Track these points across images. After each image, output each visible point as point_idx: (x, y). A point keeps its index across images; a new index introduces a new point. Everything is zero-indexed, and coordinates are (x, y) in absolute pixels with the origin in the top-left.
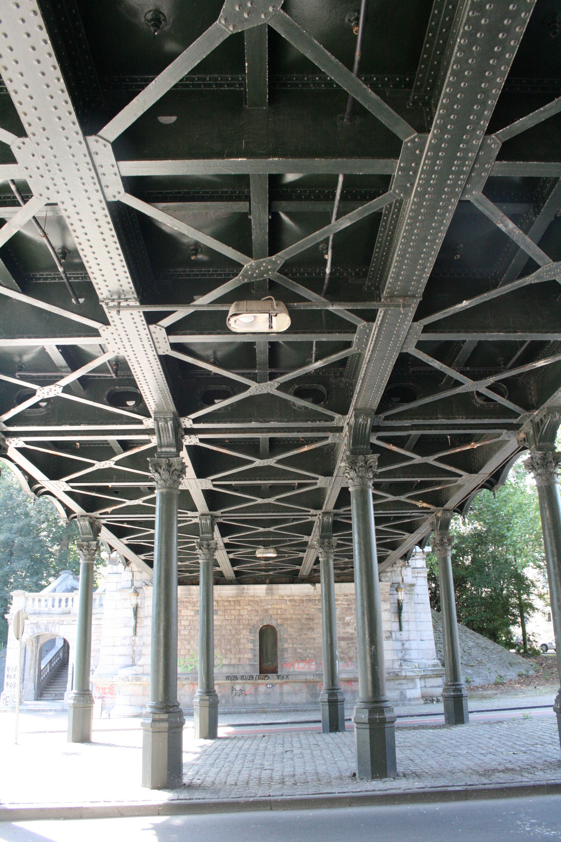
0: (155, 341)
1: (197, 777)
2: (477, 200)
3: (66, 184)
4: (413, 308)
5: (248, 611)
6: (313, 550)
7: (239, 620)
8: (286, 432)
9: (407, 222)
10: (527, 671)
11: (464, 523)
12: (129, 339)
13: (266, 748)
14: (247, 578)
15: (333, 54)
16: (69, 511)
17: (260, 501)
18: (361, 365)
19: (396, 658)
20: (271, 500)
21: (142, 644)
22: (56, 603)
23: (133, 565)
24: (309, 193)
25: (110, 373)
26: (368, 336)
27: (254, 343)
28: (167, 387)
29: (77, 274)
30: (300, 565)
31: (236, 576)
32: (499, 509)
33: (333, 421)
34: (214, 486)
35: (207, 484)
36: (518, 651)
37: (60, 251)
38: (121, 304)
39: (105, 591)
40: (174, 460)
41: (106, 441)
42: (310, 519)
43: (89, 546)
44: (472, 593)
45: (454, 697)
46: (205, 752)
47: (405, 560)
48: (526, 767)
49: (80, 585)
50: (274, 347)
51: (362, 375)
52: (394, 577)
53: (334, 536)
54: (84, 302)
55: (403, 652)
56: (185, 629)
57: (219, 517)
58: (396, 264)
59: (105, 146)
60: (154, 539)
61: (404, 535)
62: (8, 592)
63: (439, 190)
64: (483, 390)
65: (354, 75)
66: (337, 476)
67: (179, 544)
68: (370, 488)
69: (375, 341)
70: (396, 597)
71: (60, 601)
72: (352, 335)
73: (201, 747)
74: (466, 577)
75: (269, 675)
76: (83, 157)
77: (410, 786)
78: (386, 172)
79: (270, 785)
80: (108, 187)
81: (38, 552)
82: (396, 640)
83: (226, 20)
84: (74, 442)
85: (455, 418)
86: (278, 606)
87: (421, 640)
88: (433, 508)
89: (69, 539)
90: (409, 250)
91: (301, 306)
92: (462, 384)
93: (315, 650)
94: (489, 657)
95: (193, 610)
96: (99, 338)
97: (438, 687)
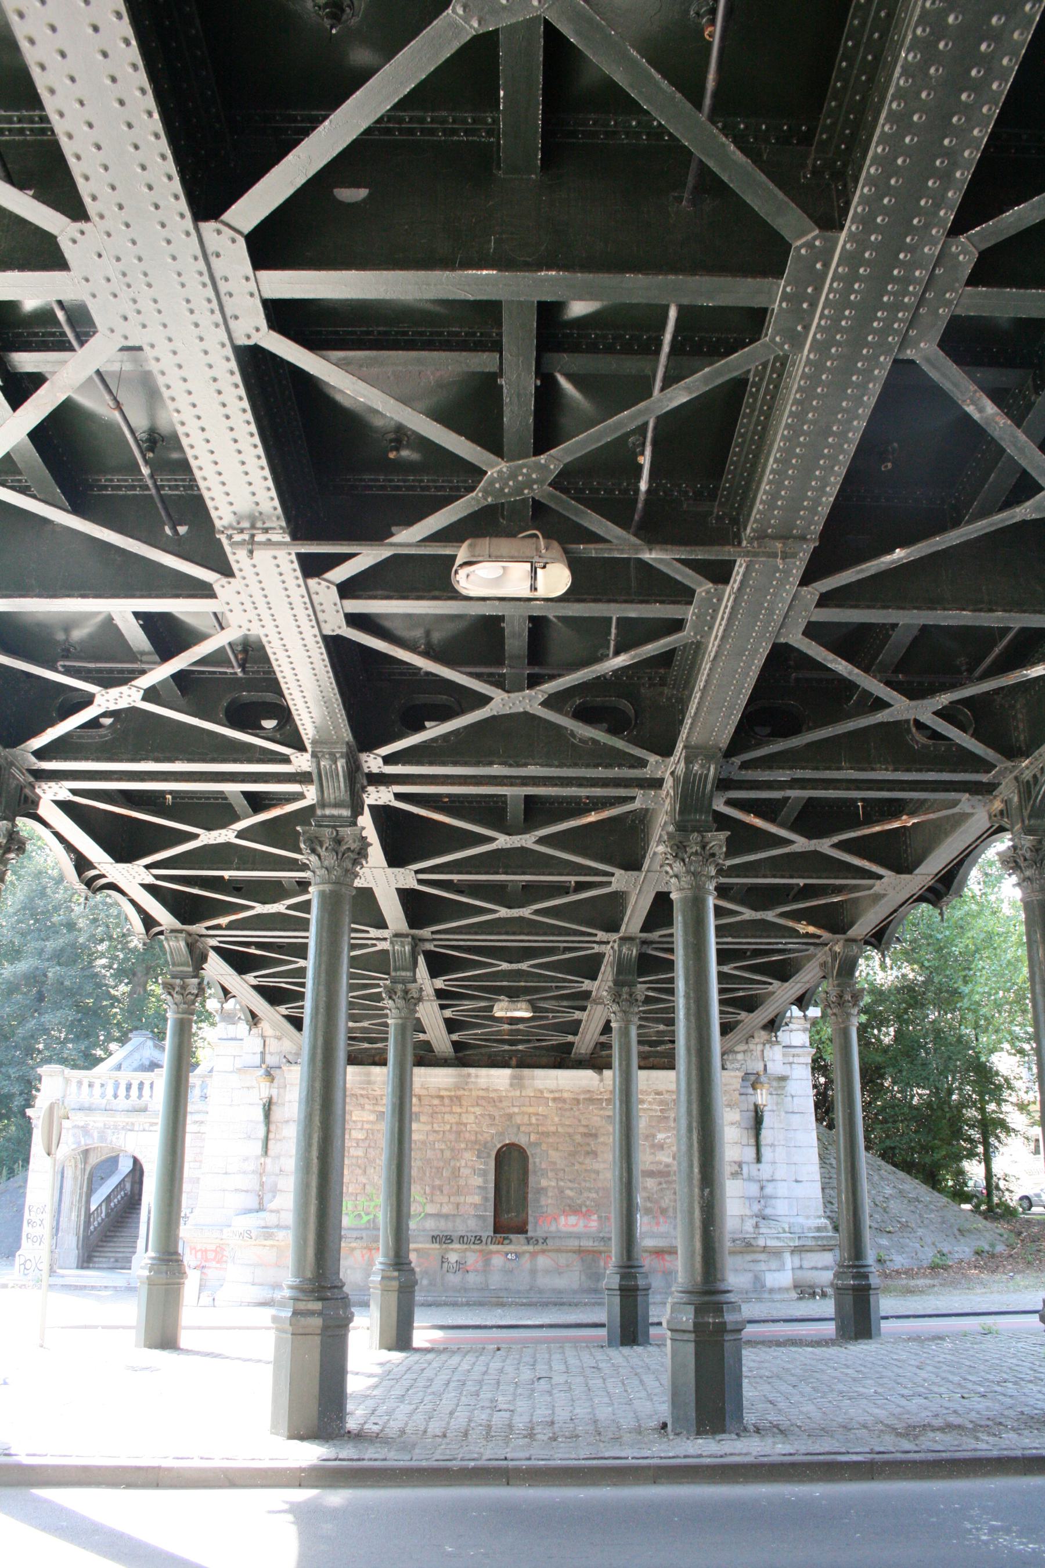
0: (318, 608)
1: (373, 1419)
2: (928, 360)
3: (159, 312)
4: (801, 560)
5: (476, 1117)
6: (600, 1007)
7: (459, 1133)
8: (556, 785)
9: (795, 398)
10: (992, 1245)
11: (883, 966)
12: (268, 603)
13: (501, 1371)
14: (476, 1055)
15: (665, 76)
16: (149, 922)
17: (504, 912)
18: (701, 664)
19: (748, 1212)
20: (526, 912)
21: (278, 1172)
22: (122, 1092)
23: (264, 1025)
24: (614, 338)
25: (233, 667)
26: (716, 611)
27: (501, 618)
28: (338, 696)
29: (176, 480)
30: (575, 1033)
31: (456, 1052)
32: (950, 942)
33: (645, 767)
34: (420, 882)
35: (407, 877)
36: (977, 1207)
37: (144, 436)
38: (257, 539)
39: (211, 1071)
40: (347, 832)
41: (222, 792)
42: (597, 949)
43: (184, 987)
44: (893, 1097)
45: (855, 1289)
46: (388, 1375)
47: (772, 1031)
48: (983, 1423)
49: (165, 1058)
50: (538, 625)
51: (701, 683)
52: (749, 1062)
53: (641, 983)
54: (187, 532)
55: (762, 1202)
56: (358, 1146)
57: (427, 940)
58: (771, 477)
59: (234, 241)
60: (304, 978)
61: (771, 984)
62: (33, 1068)
63: (857, 341)
64: (927, 718)
65: (703, 117)
66: (648, 871)
67: (352, 988)
68: (710, 894)
69: (729, 619)
70: (752, 1099)
71: (129, 1087)
72: (684, 607)
73: (382, 1364)
74: (884, 1068)
75: (511, 1236)
76: (192, 261)
77: (767, 1450)
78: (757, 303)
79: (507, 1441)
80: (236, 318)
81: (90, 995)
82: (750, 1179)
83: (465, 7)
84: (162, 794)
85: (873, 769)
86: (531, 1110)
87: (797, 1181)
88: (826, 935)
89: (147, 974)
90: (798, 450)
91: (592, 550)
92: (889, 705)
93: (597, 1192)
94: (921, 1216)
95: (374, 1112)
96: (214, 600)
97: (826, 1268)
